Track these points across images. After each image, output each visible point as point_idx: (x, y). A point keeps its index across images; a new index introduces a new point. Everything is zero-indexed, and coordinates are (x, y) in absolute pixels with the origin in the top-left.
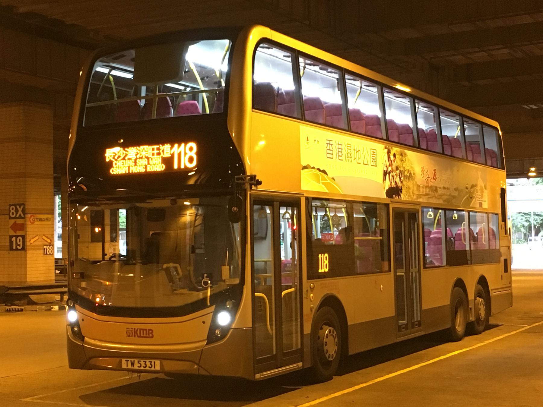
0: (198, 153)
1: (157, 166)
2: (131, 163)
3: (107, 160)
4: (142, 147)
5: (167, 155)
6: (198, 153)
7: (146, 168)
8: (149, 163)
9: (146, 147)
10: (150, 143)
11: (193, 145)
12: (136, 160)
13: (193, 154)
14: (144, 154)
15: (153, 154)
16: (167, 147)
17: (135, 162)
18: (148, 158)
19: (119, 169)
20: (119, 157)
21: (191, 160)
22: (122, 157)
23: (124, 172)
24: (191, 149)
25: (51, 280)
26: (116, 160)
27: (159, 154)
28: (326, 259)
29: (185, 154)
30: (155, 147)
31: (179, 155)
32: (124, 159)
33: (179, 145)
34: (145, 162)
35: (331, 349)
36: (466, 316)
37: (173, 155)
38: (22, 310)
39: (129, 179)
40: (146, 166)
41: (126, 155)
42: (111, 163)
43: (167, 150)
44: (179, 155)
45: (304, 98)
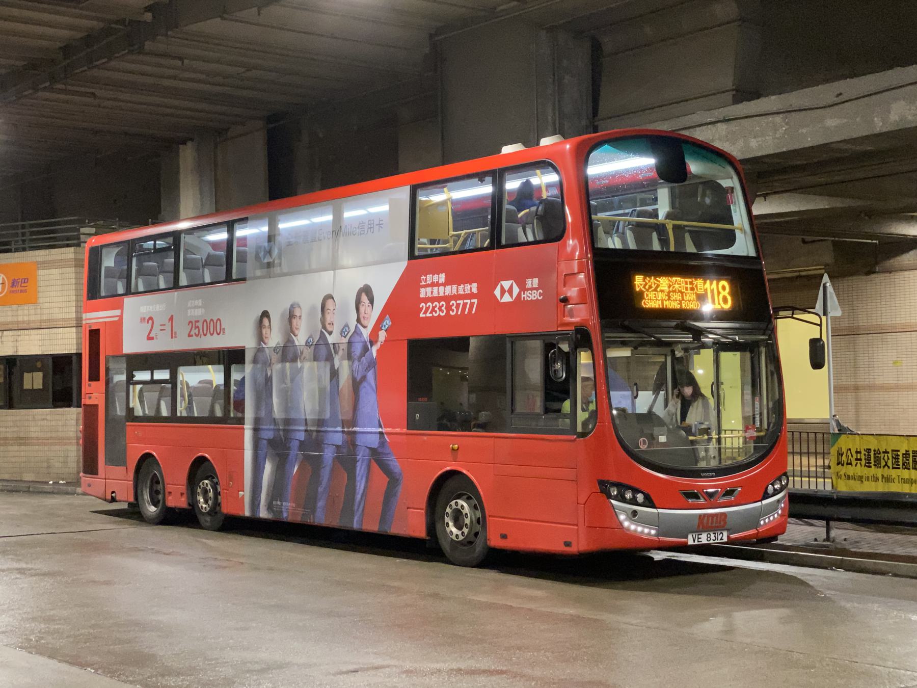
3: (638, 289)
4: (674, 279)
6: (732, 294)
7: (681, 304)
12: (669, 292)
13: (726, 293)
18: (682, 293)
19: (651, 301)
20: (650, 287)
21: (725, 300)
22: (654, 287)
23: (657, 306)
24: (724, 288)
25: (78, 414)
29: (719, 293)
30: (688, 280)
32: (655, 290)
35: (165, 412)
36: (372, 387)
37: (706, 290)
38: (225, 567)
41: (658, 286)
42: (641, 294)
45: (226, 229)
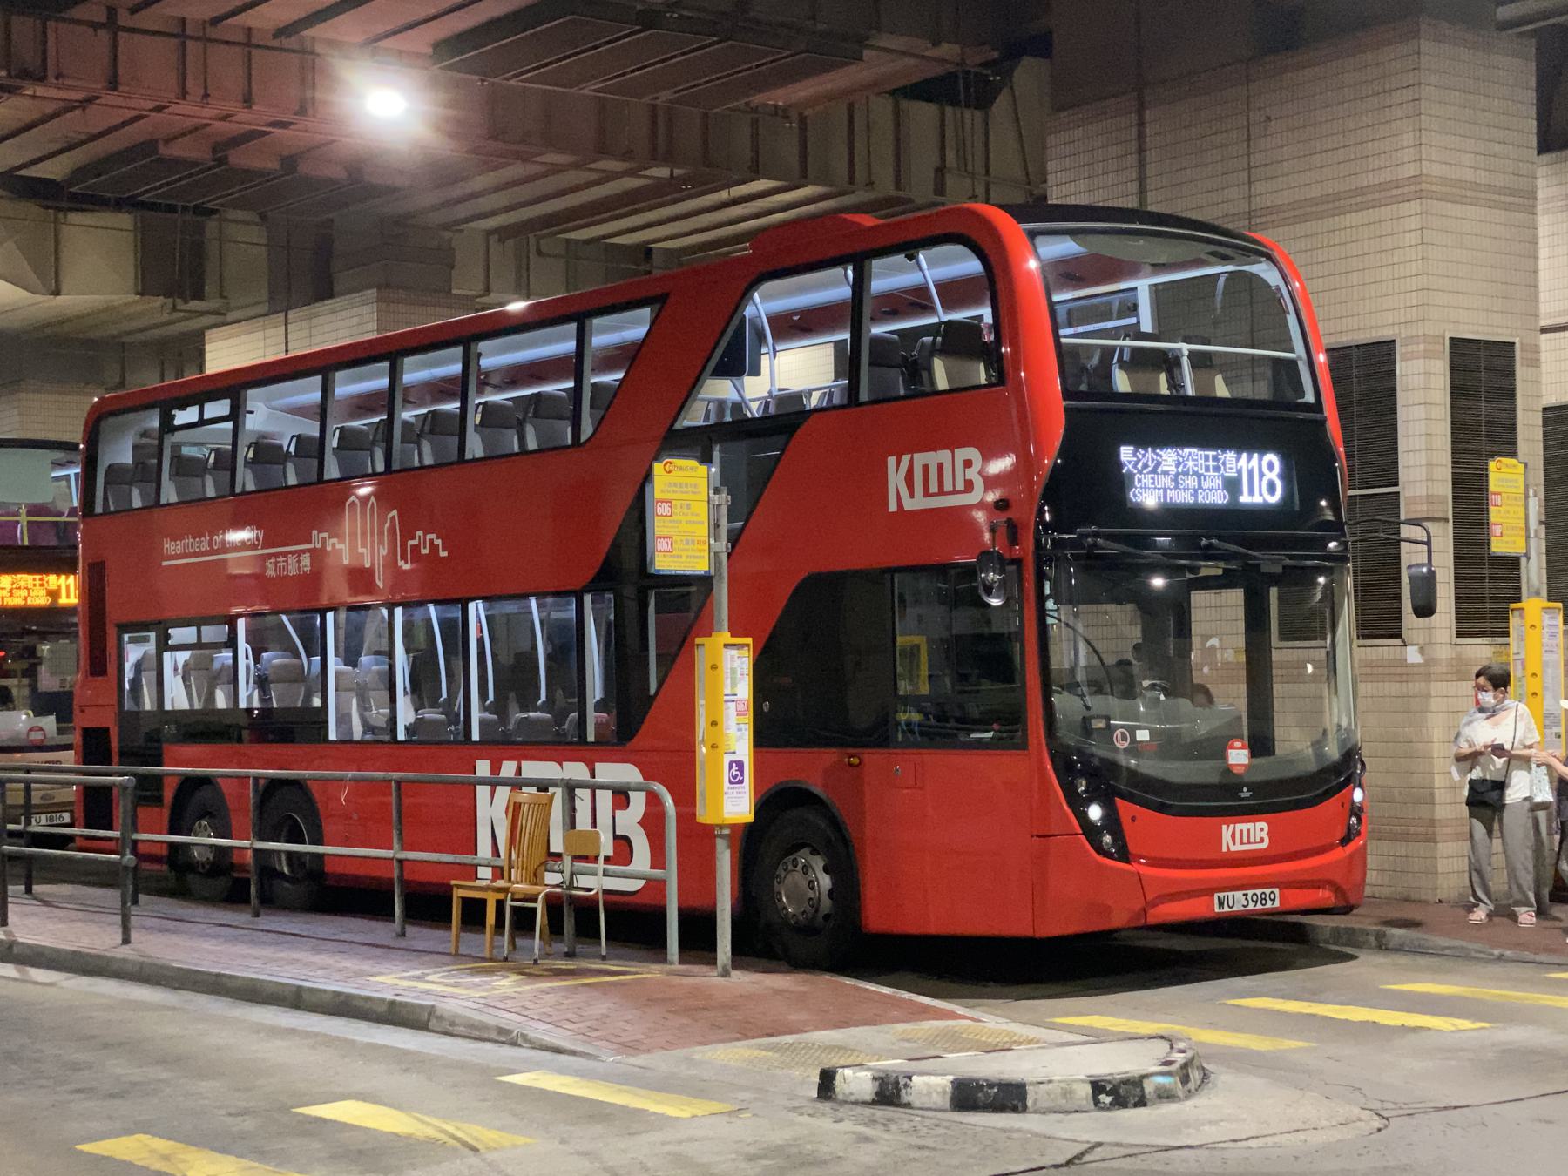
0: (1282, 476)
1: (40, 599)
2: (1167, 481)
4: (1187, 451)
5: (53, 587)
6: (1285, 476)
8: (1200, 487)
9: (25, 576)
10: (1204, 444)
11: (1271, 457)
13: (1274, 475)
14: (22, 584)
15: (1207, 469)
16: (1230, 455)
17: (1176, 480)
18: (1199, 476)
19: (1147, 495)
24: (1271, 466)
26: (1140, 472)
27: (1217, 469)
28: (736, 781)
29: (1262, 475)
30: (1211, 453)
31: (1250, 473)
32: (1154, 471)
33: (1249, 459)
34: (1191, 482)
37: (1239, 472)
39: (1174, 516)
40: (1196, 491)
41: (1159, 464)
43: (53, 580)
44: (1250, 473)
